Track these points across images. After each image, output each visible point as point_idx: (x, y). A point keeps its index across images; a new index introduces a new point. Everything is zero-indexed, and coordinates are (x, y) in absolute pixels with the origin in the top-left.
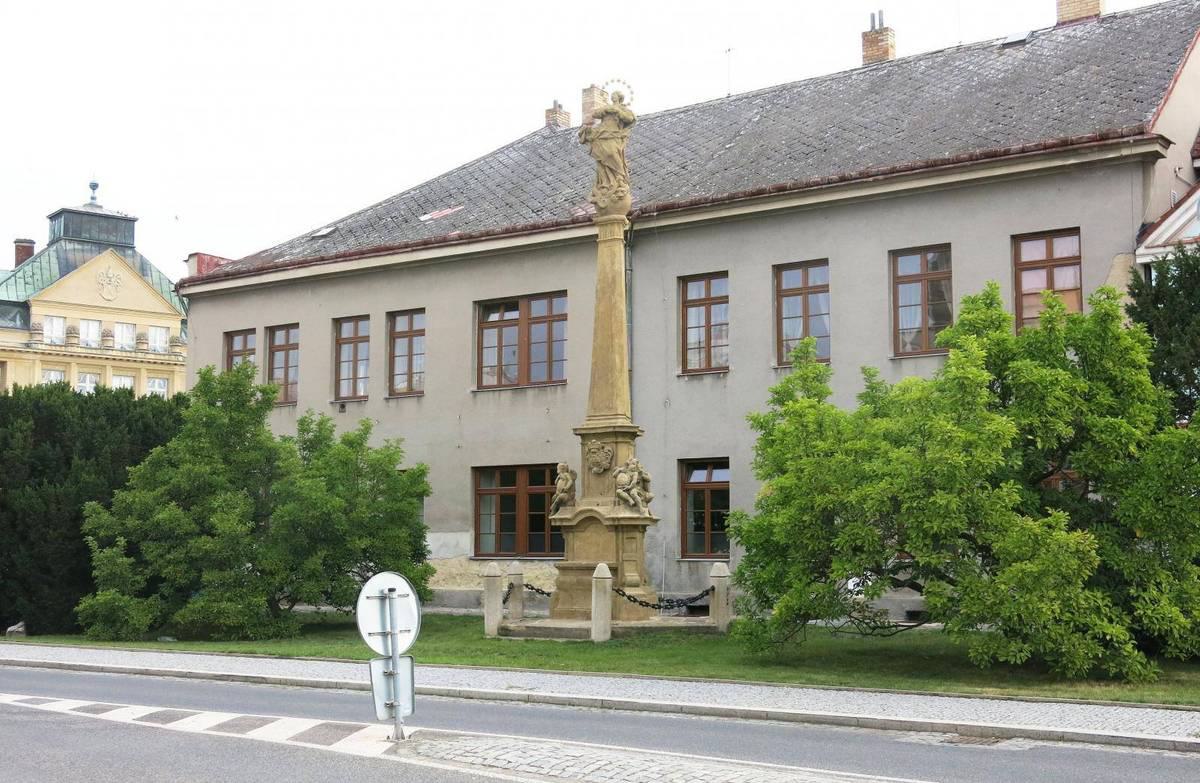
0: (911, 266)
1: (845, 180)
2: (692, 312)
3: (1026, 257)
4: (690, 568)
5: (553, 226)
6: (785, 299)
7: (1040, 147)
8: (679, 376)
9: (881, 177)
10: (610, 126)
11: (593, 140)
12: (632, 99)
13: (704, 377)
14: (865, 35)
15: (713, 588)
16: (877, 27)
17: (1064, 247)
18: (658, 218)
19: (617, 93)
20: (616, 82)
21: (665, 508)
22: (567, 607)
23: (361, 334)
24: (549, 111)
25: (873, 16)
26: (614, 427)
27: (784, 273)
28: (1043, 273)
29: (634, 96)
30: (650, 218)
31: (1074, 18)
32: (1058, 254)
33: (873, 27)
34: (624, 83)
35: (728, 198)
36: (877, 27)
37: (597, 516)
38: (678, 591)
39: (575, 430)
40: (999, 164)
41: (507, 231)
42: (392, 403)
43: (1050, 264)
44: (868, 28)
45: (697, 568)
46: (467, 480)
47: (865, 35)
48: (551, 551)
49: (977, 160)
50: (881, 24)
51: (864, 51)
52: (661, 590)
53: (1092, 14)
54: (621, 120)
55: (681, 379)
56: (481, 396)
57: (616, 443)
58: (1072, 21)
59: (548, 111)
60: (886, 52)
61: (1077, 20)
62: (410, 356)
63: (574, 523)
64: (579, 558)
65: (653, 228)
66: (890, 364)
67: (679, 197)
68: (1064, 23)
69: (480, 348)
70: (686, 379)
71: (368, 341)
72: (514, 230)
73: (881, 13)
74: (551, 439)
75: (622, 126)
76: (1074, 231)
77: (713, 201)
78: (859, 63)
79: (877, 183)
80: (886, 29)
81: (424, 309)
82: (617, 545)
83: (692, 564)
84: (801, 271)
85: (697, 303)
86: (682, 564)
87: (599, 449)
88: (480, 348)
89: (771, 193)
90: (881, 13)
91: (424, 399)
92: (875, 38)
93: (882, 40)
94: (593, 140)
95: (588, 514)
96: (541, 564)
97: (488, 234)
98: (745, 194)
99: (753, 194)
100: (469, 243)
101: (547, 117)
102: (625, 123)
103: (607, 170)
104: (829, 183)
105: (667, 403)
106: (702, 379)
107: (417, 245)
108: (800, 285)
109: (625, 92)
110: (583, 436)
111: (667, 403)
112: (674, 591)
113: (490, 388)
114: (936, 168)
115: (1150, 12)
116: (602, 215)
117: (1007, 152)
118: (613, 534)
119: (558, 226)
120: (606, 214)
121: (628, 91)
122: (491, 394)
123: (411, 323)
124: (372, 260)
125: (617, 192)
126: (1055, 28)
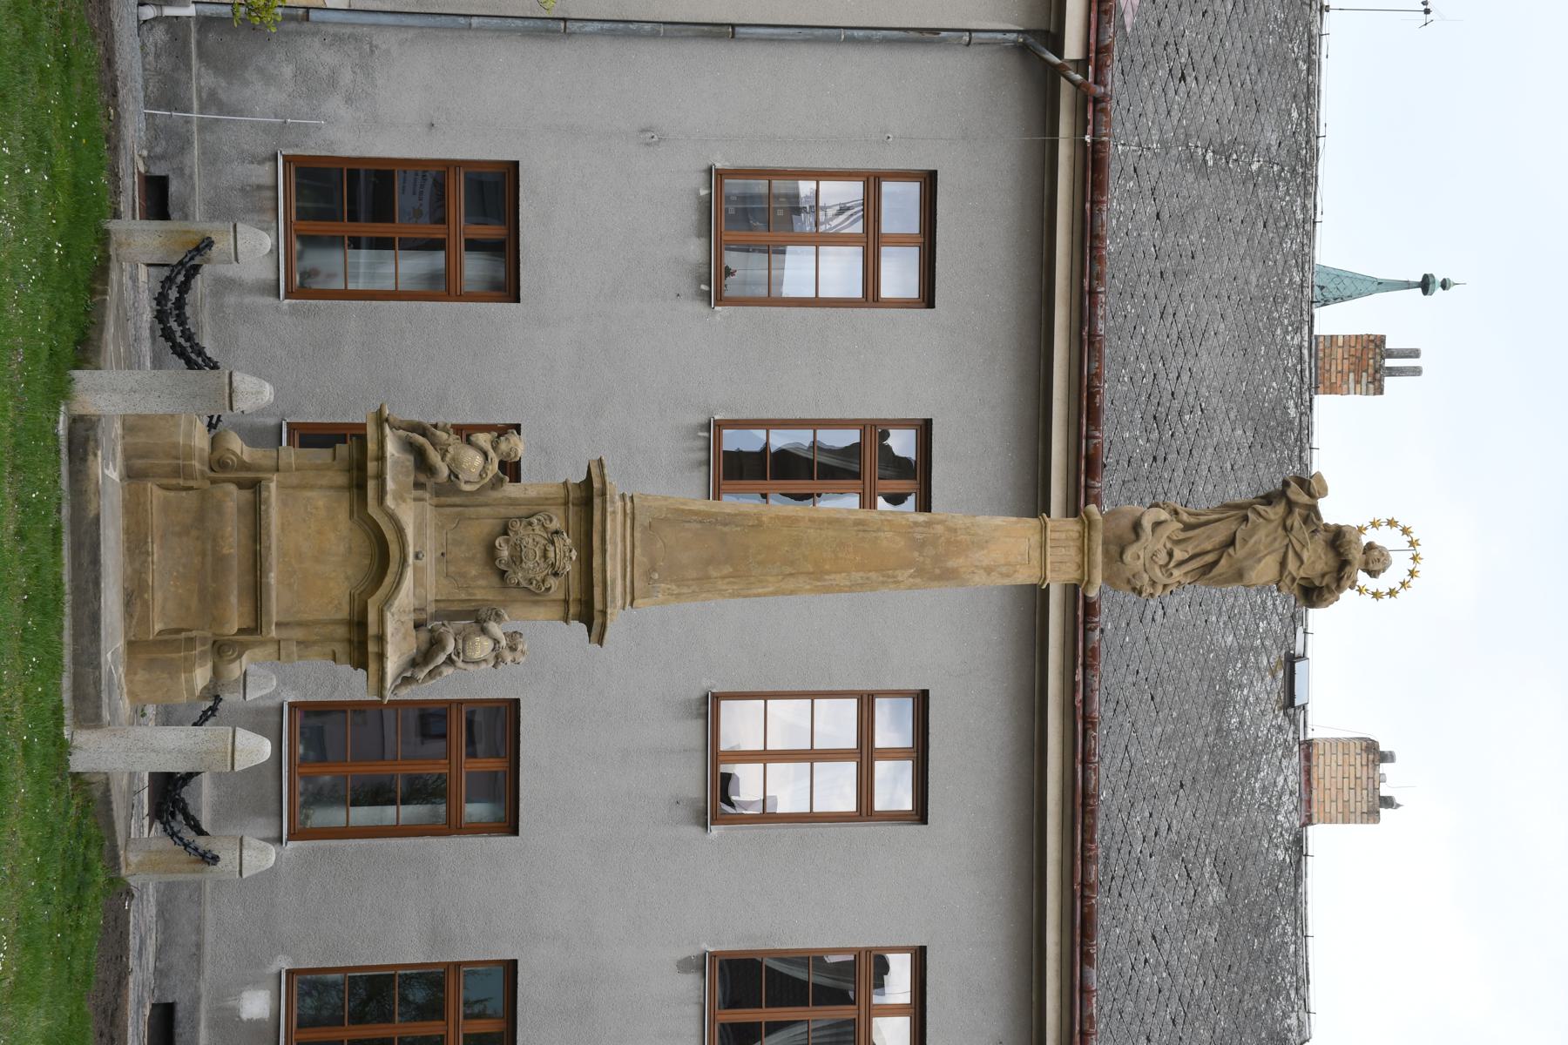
0: (902, 443)
1: (1086, 614)
3: (882, 707)
4: (260, 187)
7: (1087, 1026)
9: (1080, 696)
11: (1287, 530)
13: (704, 240)
14: (1382, 339)
15: (215, 859)
16: (1389, 363)
17: (899, 274)
18: (1079, 144)
22: (156, 519)
25: (1414, 353)
26: (604, 613)
28: (850, 742)
30: (1081, 125)
31: (1314, 775)
32: (881, 767)
33: (1391, 354)
34: (1414, 558)
35: (1093, 334)
36: (1389, 363)
38: (204, 153)
45: (261, 210)
47: (1382, 339)
49: (1083, 897)
50: (1393, 372)
53: (1314, 810)
57: (566, 602)
58: (1308, 772)
60: (1332, 389)
61: (1309, 782)
63: (372, 508)
64: (284, 503)
65: (1054, 131)
67: (1116, 206)
70: (703, 192)
73: (1416, 371)
76: (927, 298)
77: (1093, 293)
79: (1069, 687)
82: (316, 623)
83: (269, 194)
86: (268, 167)
87: (553, 565)
89: (1088, 438)
93: (1358, 382)
94: (1287, 530)
98: (1095, 376)
99: (1091, 396)
103: (1209, 558)
105: (650, 137)
106: (698, 716)
108: (880, 742)
109: (1384, 582)
111: (650, 137)
112: (202, 141)
114: (1081, 627)
116: (1105, 543)
117: (1087, 958)
118: (344, 613)
120: (1106, 553)
125: (1153, 583)
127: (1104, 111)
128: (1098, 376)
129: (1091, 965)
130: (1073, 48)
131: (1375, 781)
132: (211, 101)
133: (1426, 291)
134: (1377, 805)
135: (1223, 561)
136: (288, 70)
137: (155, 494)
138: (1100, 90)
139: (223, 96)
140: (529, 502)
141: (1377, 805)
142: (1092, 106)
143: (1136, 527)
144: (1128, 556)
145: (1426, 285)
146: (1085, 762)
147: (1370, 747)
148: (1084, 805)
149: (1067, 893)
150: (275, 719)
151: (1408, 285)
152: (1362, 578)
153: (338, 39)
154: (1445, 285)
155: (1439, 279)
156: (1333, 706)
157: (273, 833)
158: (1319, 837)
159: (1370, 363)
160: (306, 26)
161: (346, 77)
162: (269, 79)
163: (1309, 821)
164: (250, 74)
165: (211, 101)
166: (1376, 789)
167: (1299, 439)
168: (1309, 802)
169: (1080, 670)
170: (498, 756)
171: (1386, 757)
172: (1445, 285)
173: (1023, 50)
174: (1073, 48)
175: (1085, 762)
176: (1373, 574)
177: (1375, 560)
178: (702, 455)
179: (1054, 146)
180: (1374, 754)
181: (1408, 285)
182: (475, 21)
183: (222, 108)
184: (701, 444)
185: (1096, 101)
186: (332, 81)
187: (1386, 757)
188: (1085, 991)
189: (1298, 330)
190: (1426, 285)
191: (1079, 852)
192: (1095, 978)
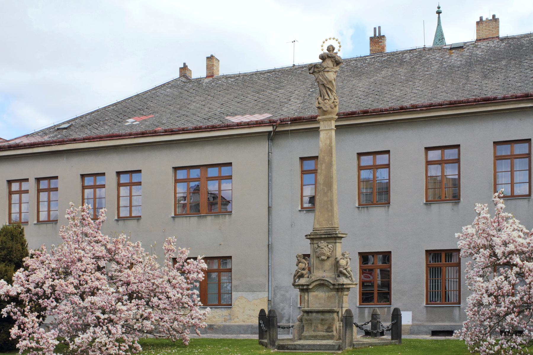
2: (87, 191)
5: (225, 127)
6: (41, 193)
8: (300, 211)
9: (424, 108)
10: (329, 63)
12: (339, 51)
13: (432, 205)
16: (377, 35)
17: (382, 160)
19: (332, 46)
20: (332, 39)
21: (354, 279)
23: (52, 186)
24: (181, 69)
25: (375, 29)
27: (178, 171)
29: (322, 43)
30: (286, 125)
31: (485, 37)
32: (378, 163)
36: (377, 35)
37: (327, 283)
39: (306, 236)
40: (490, 105)
41: (196, 129)
42: (121, 223)
43: (375, 167)
44: (373, 35)
46: (422, 260)
48: (363, 302)
49: (478, 102)
51: (371, 46)
52: (289, 323)
54: (336, 61)
55: (302, 212)
56: (177, 220)
58: (484, 39)
59: (181, 69)
60: (383, 48)
61: (487, 39)
62: (49, 201)
65: (288, 131)
66: (425, 207)
68: (480, 40)
69: (10, 204)
70: (305, 212)
71: (231, 179)
72: (200, 128)
73: (379, 27)
74: (222, 243)
75: (335, 65)
76: (388, 152)
78: (368, 53)
79: (422, 111)
80: (384, 36)
81: (28, 179)
84: (372, 156)
85: (16, 192)
88: (10, 204)
90: (379, 27)
91: (142, 221)
92: (377, 40)
93: (381, 42)
95: (322, 282)
96: (216, 310)
97: (183, 130)
99: (349, 114)
100: (171, 134)
101: (180, 72)
102: (337, 63)
104: (394, 110)
106: (430, 206)
107: (137, 134)
109: (336, 45)
110: (312, 239)
113: (125, 219)
115: (528, 37)
117: (495, 99)
119: (213, 128)
121: (324, 45)
122: (184, 219)
123: (20, 186)
124: (108, 142)
126: (476, 42)
127: (283, 120)
128: (344, 113)
129: (496, 98)
130: (270, 129)
131: (488, 21)
132: (288, 320)
133: (441, 13)
134: (495, 20)
135: (328, 86)
136: (281, 305)
137: (305, 334)
138: (279, 122)
139: (287, 318)
140: (313, 252)
141: (495, 20)
142: (283, 122)
143: (319, 108)
144: (325, 109)
145: (439, 13)
146: (441, 105)
147: (478, 23)
148: (453, 104)
149: (477, 106)
150: (429, 308)
151: (439, 17)
152: (335, 51)
153: (275, 294)
154: (439, 8)
155: (437, 9)
156: (468, 35)
157: (458, 309)
158: (502, 34)
159: (377, 40)
160: (272, 301)
161: (282, 292)
162: (283, 309)
163: (498, 37)
164: (282, 312)
165: (288, 320)
166: (491, 20)
167: (393, 55)
168: (492, 38)
169: (417, 109)
170: (226, 263)
171: (481, 18)
172: (439, 8)
173: (272, 140)
174: (270, 129)
175: (441, 105)
176: (334, 49)
177: (331, 49)
178: (365, 209)
179: (291, 130)
180: (480, 22)
181: (439, 17)
182: (270, 265)
183: (289, 319)
184: (363, 209)
185: (281, 122)
186: (283, 295)
187: (481, 18)
188: (504, 98)
189: (366, 59)
190: (439, 13)
191: (467, 103)
192: (500, 96)
